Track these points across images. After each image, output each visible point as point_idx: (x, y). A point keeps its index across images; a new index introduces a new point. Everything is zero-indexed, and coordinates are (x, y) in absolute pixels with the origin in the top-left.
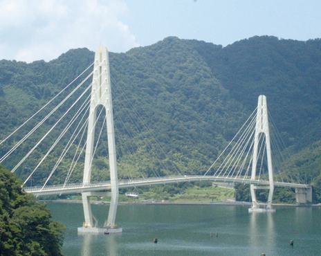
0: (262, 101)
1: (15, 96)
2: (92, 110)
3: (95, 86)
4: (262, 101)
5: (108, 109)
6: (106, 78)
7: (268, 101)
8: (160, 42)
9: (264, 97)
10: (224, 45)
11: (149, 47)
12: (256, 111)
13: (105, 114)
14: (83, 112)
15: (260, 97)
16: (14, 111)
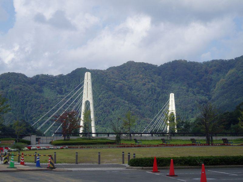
0: (172, 96)
1: (48, 94)
2: (40, 137)
3: (85, 91)
4: (172, 96)
5: (91, 102)
6: (90, 87)
7: (175, 96)
8: (124, 64)
9: (173, 94)
10: (159, 65)
11: (121, 66)
12: (169, 102)
13: (90, 105)
14: (80, 103)
15: (171, 94)
16: (47, 101)
